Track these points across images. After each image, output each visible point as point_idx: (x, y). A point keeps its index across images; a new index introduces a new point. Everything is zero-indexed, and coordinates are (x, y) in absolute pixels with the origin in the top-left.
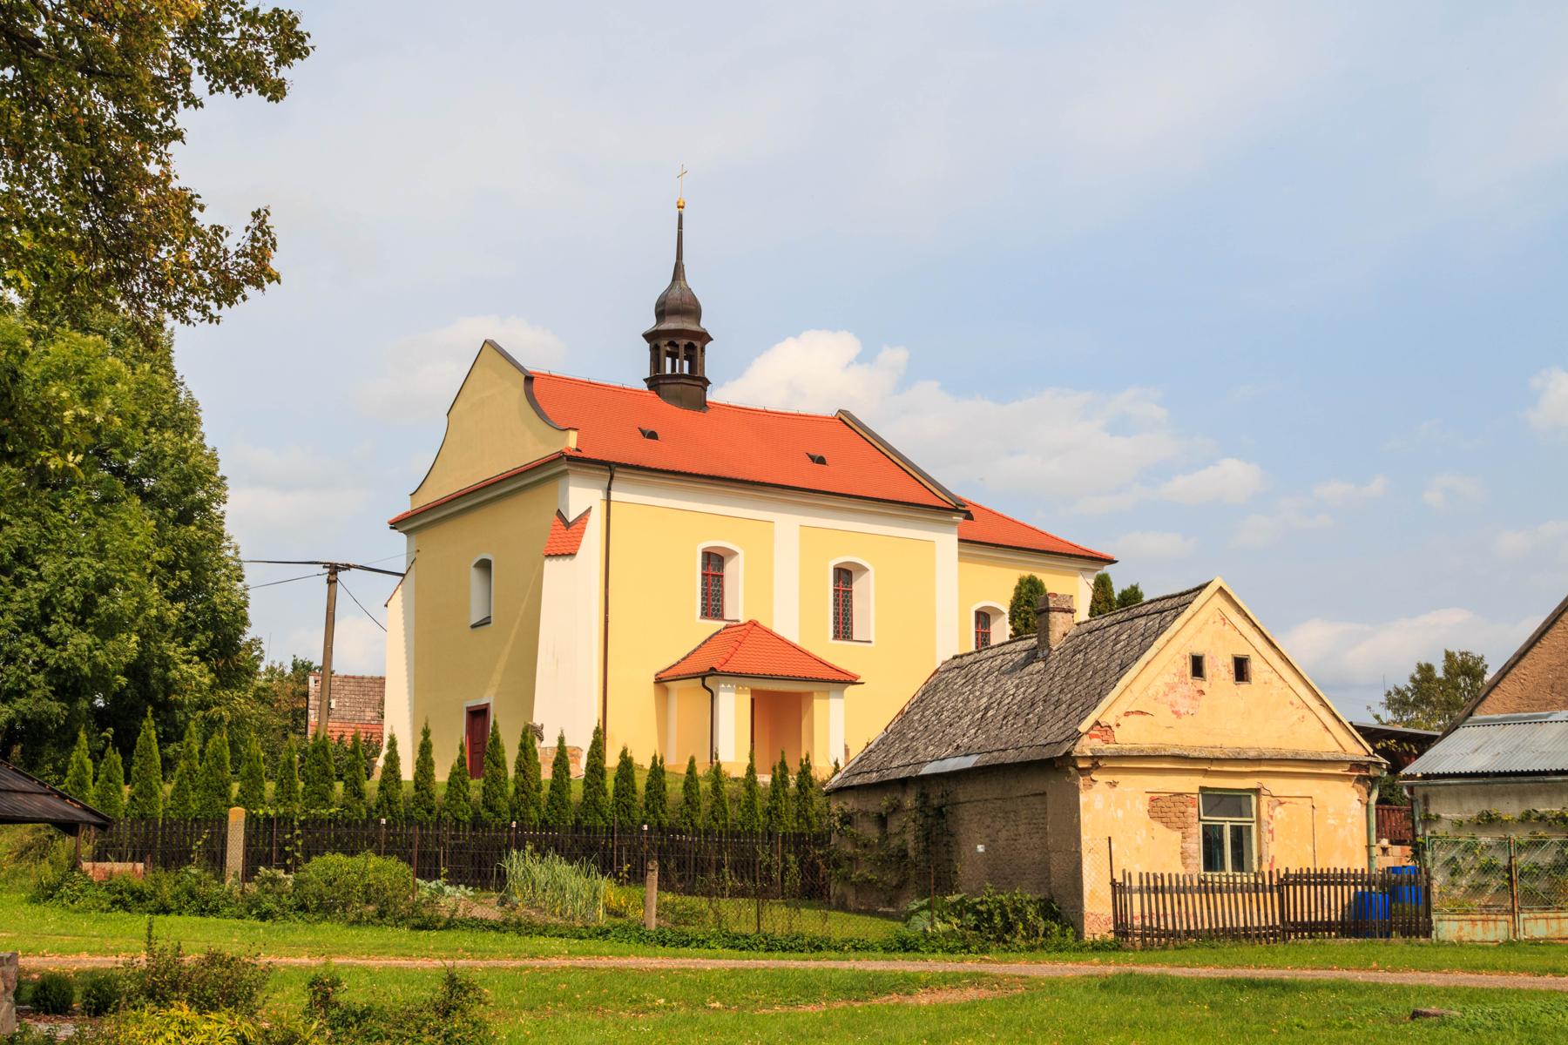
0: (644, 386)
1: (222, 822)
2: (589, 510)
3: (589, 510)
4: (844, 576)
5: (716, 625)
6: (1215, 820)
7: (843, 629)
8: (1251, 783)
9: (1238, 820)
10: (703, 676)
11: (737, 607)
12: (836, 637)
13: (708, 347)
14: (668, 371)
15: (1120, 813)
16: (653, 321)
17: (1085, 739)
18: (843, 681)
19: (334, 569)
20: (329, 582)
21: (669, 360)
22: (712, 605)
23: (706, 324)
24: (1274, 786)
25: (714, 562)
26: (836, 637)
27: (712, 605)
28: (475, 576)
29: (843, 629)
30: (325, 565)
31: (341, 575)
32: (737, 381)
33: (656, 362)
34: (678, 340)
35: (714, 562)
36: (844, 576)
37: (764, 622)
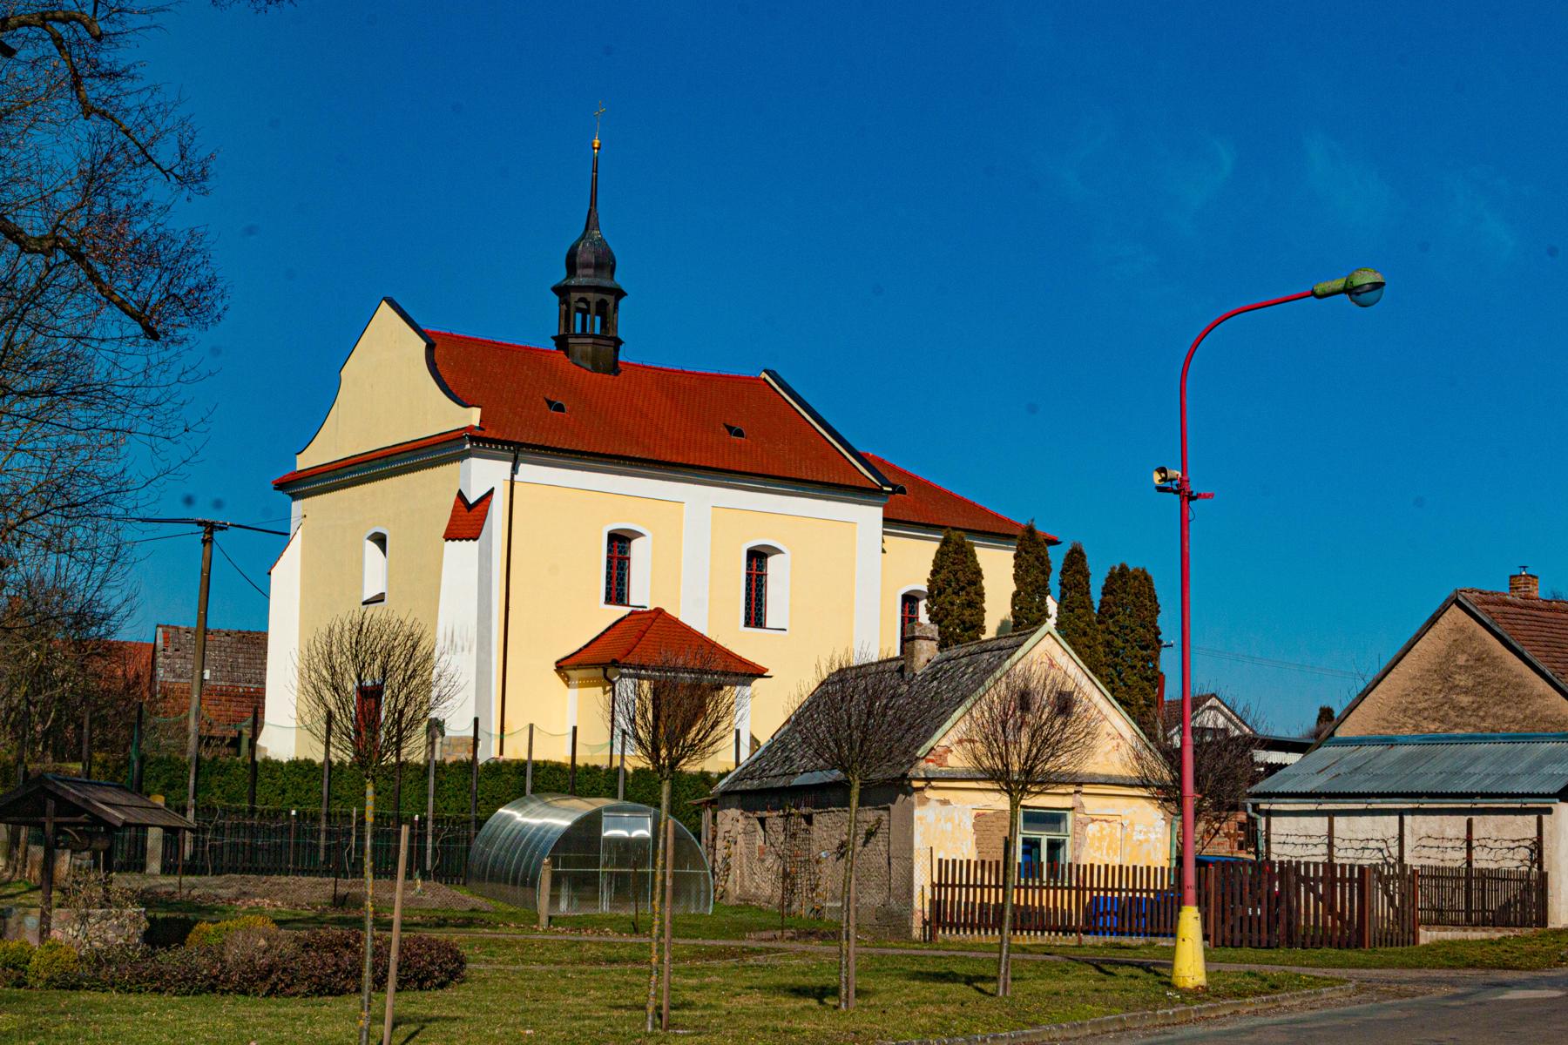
0: (552, 345)
1: (398, 834)
2: (491, 492)
3: (491, 492)
4: (758, 557)
5: (620, 611)
6: (1033, 834)
7: (755, 616)
8: (1067, 802)
9: (1054, 836)
10: (605, 667)
11: (642, 594)
12: (747, 624)
13: (622, 303)
14: (578, 330)
15: (949, 826)
16: (564, 273)
17: (922, 764)
18: (751, 673)
19: (210, 527)
20: (204, 542)
21: (579, 316)
22: (616, 591)
23: (620, 279)
24: (1092, 805)
25: (619, 542)
26: (747, 624)
27: (616, 591)
28: (372, 548)
29: (755, 616)
30: (200, 523)
31: (217, 535)
32: (649, 335)
33: (567, 318)
34: (589, 291)
35: (619, 542)
36: (758, 557)
37: (669, 611)
